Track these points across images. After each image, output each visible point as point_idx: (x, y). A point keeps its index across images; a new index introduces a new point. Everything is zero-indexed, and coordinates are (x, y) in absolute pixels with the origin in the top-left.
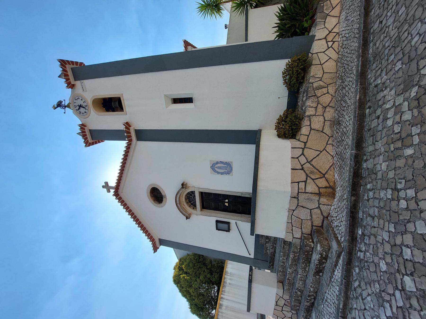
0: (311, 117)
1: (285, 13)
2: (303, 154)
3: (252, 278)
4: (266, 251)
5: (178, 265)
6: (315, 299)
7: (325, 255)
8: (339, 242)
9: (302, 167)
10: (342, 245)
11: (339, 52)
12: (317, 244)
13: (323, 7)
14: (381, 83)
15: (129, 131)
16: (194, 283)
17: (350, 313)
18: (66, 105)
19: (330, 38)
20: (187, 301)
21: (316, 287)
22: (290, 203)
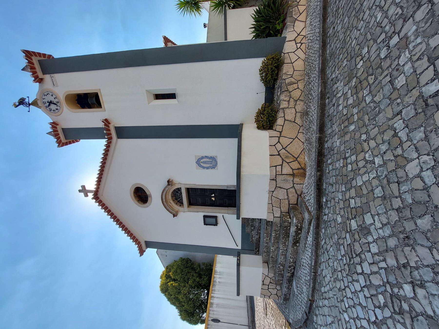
0: (285, 109)
1: (260, 15)
2: (279, 142)
3: (239, 262)
4: (252, 238)
5: (165, 273)
6: (294, 269)
7: (300, 227)
8: (309, 212)
9: (279, 153)
10: (312, 214)
11: (306, 52)
12: (293, 218)
13: (292, 12)
14: (335, 77)
15: (108, 128)
16: (182, 289)
17: (319, 267)
18: (30, 103)
19: (298, 40)
20: (177, 309)
21: (295, 257)
22: (270, 185)
